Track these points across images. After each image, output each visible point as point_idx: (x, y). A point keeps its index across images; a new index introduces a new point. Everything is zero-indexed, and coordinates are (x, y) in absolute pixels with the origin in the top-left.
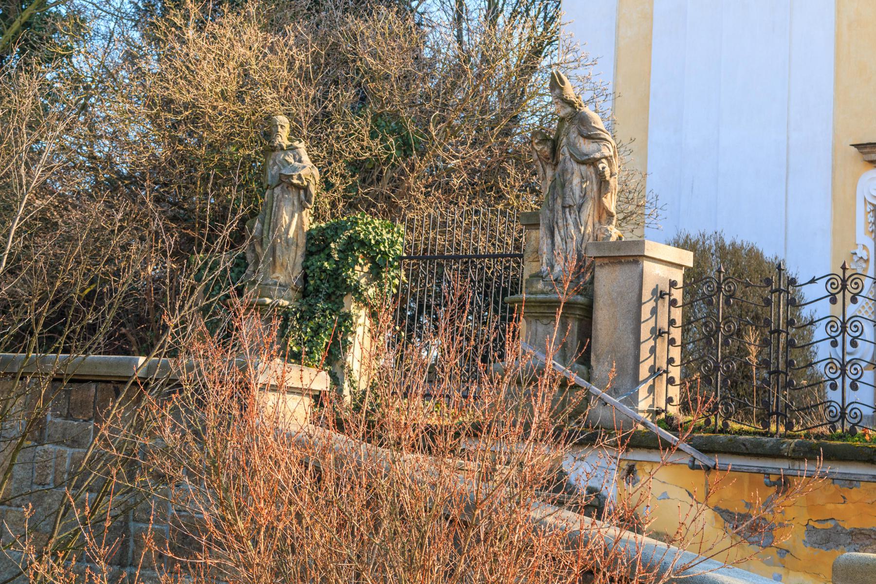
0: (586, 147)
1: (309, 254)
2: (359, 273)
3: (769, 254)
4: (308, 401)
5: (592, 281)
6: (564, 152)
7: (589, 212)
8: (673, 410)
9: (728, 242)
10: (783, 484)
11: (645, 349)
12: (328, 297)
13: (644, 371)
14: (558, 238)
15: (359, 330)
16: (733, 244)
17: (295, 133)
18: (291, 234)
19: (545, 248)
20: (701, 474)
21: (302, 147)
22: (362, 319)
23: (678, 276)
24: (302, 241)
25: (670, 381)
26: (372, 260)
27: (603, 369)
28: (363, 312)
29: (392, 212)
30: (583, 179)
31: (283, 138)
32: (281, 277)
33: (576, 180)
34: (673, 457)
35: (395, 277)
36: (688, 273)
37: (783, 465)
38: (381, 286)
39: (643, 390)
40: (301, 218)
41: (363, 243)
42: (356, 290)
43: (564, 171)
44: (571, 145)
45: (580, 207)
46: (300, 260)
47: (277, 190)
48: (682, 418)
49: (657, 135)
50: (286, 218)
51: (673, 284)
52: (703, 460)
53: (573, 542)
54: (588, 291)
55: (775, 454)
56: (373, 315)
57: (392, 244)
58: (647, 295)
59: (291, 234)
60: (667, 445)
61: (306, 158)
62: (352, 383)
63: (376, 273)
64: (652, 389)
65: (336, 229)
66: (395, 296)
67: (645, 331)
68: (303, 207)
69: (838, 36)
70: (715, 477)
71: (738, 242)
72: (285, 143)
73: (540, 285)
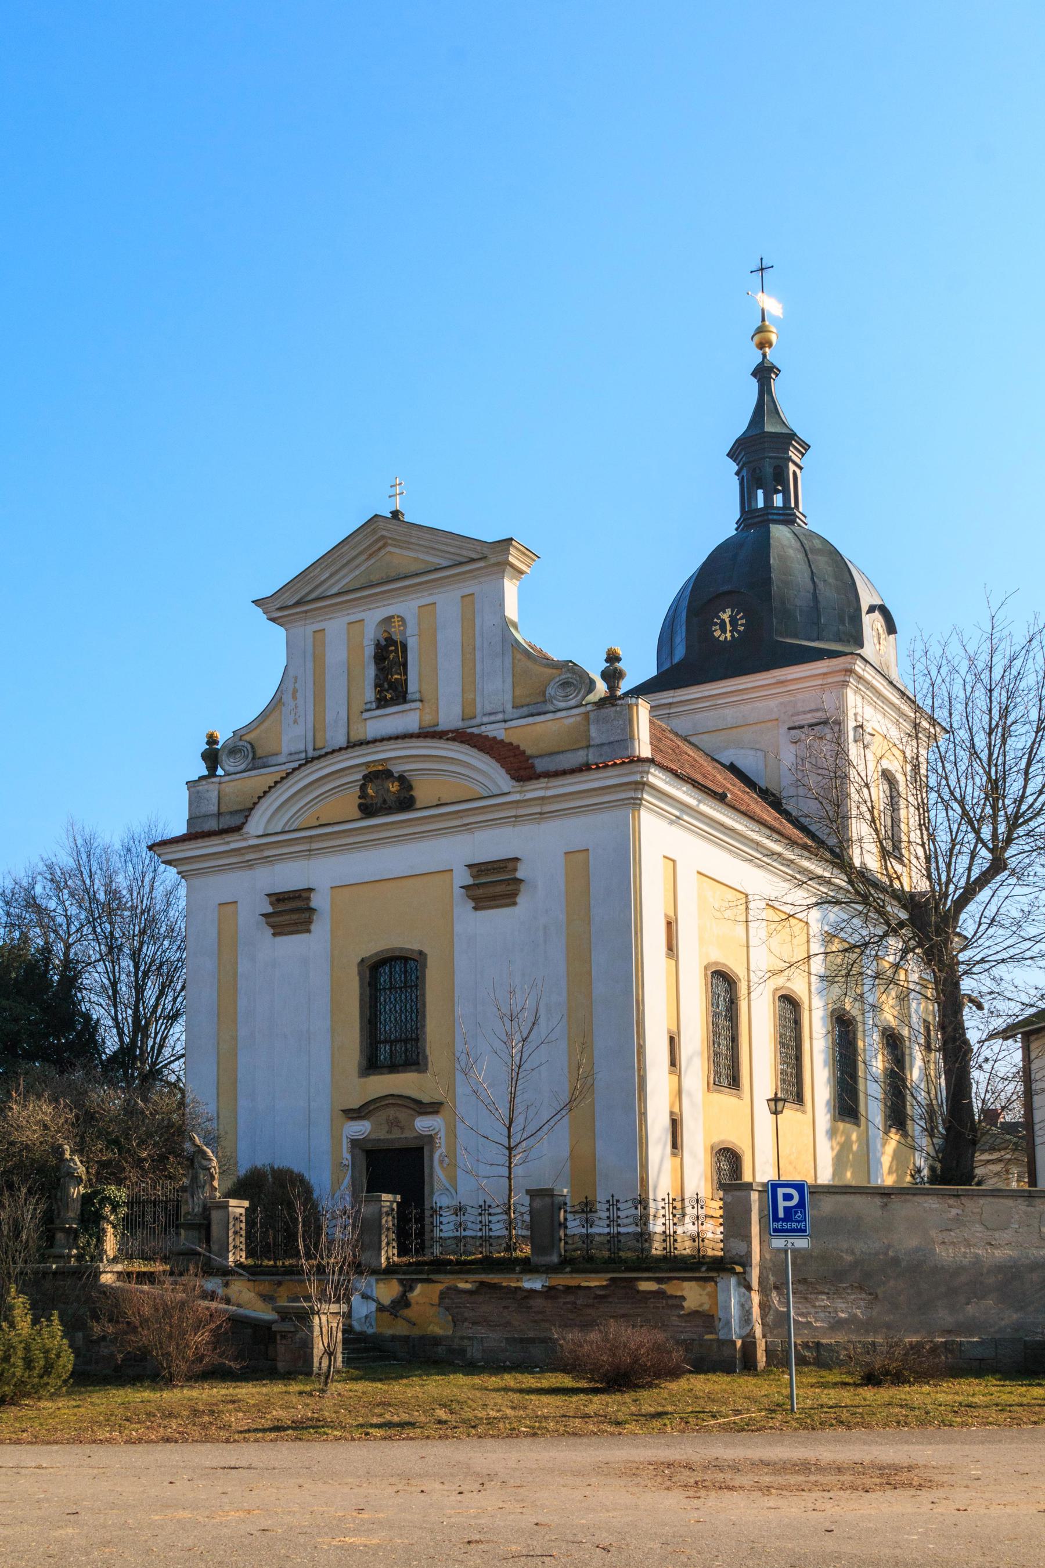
0: (205, 1163)
1: (83, 1204)
2: (108, 1208)
3: (296, 1170)
4: (116, 1275)
5: (210, 1214)
6: (196, 1164)
7: (207, 1187)
8: (243, 1260)
9: (276, 1167)
10: (280, 1284)
11: (231, 1239)
12: (94, 1222)
13: (231, 1247)
14: (195, 1199)
15: (108, 1234)
16: (279, 1168)
17: (72, 1152)
18: (75, 1196)
19: (190, 1202)
20: (251, 1283)
21: (76, 1158)
22: (110, 1230)
23: (242, 1211)
24: (80, 1198)
25: (241, 1250)
26: (112, 1204)
27: (215, 1247)
28: (110, 1226)
29: (119, 1182)
30: (204, 1176)
31: (67, 1156)
32: (71, 1214)
33: (202, 1176)
34: (242, 1278)
35: (123, 1211)
36: (247, 1209)
37: (279, 1278)
38: (116, 1215)
39: (230, 1254)
40: (79, 1189)
41: (109, 1198)
42: (106, 1218)
43: (197, 1173)
44: (199, 1162)
45: (204, 1187)
46: (79, 1207)
47: (67, 1178)
48: (246, 1263)
49: (243, 1103)
50: (72, 1190)
51: (241, 1215)
52: (251, 1278)
53: (208, 1308)
54: (208, 1218)
55: (276, 1274)
56: (114, 1227)
57: (121, 1197)
58: (231, 1219)
59: (75, 1196)
60: (241, 1275)
61: (78, 1163)
62: (107, 1256)
63: (114, 1210)
64: (234, 1253)
65: (96, 1193)
66: (123, 1218)
67: (231, 1233)
68: (79, 1185)
69: (333, 1055)
70: (256, 1283)
71: (281, 1167)
72: (69, 1157)
73: (189, 1217)
